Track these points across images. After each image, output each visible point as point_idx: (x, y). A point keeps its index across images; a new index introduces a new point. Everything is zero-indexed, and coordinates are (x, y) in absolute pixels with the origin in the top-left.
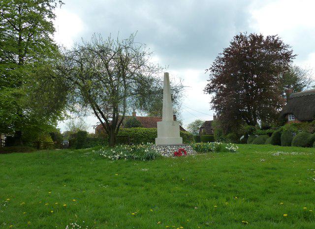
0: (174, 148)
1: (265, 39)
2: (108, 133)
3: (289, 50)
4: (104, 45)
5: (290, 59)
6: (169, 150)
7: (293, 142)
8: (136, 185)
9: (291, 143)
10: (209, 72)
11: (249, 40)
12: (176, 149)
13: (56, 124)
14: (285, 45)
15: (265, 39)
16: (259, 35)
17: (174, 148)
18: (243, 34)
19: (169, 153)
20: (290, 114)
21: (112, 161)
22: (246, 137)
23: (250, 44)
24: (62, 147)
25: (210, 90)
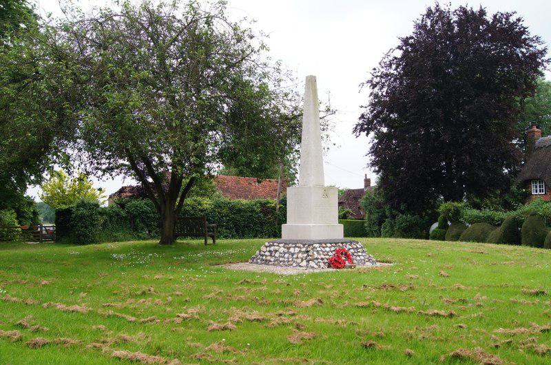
0: (328, 249)
1: (489, 18)
2: (160, 210)
3: (540, 47)
4: (363, 116)
5: (540, 69)
6: (318, 252)
7: (546, 241)
8: (399, 312)
9: (543, 241)
10: (368, 90)
11: (455, 18)
12: (330, 251)
13: (25, 188)
14: (531, 36)
15: (489, 18)
16: (476, 9)
17: (328, 249)
18: (443, 8)
19: (317, 259)
20: (535, 180)
21: (355, 282)
22: (444, 226)
23: (456, 29)
24: (39, 237)
25: (366, 126)
